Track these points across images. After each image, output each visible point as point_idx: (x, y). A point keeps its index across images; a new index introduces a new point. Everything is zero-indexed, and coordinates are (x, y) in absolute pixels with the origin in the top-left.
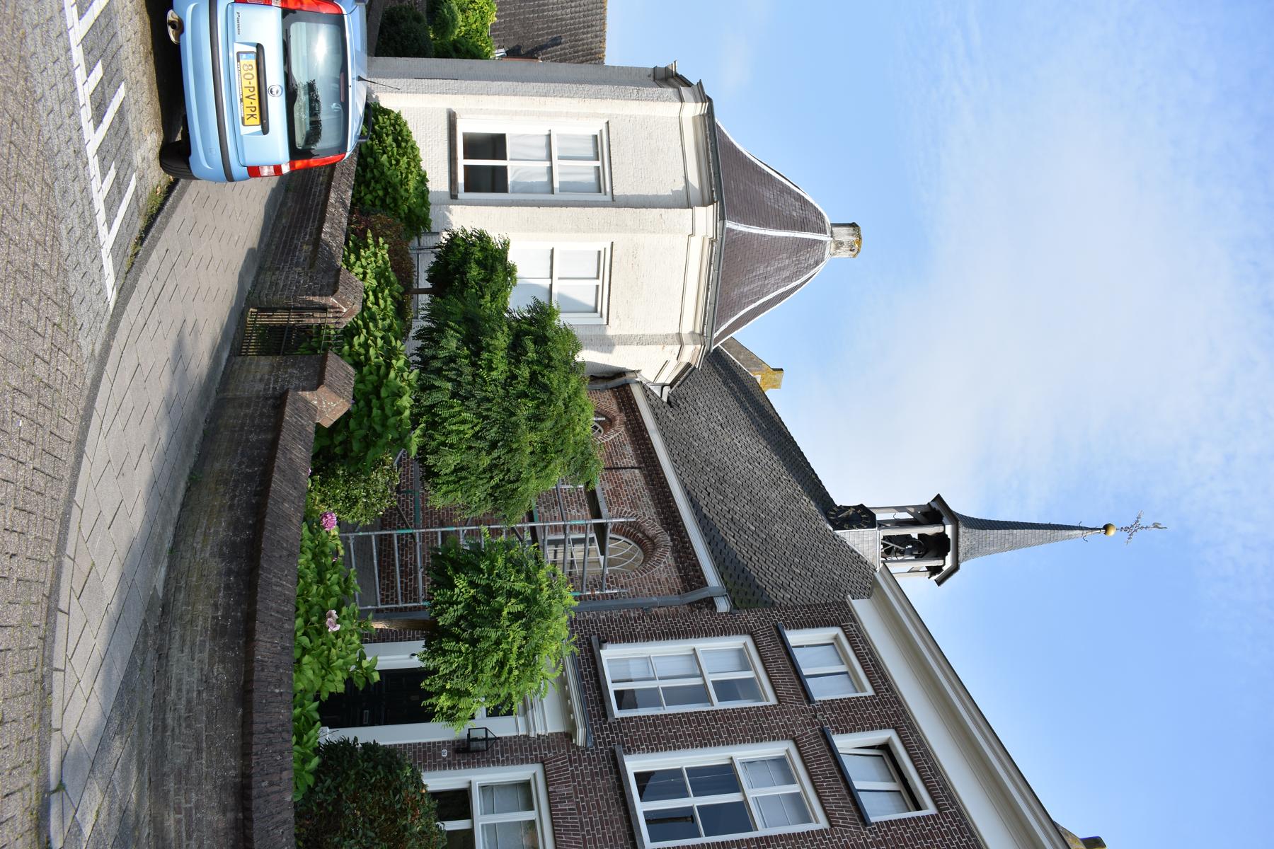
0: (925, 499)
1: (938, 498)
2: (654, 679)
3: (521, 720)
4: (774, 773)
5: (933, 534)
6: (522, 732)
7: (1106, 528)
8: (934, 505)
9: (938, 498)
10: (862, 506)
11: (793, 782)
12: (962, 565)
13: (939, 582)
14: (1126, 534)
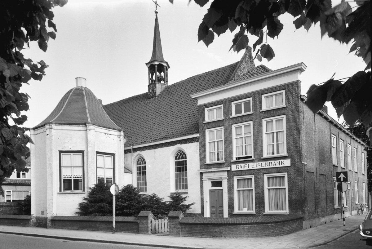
0: (146, 69)
1: (147, 64)
2: (273, 145)
3: (224, 180)
4: (270, 124)
5: (157, 68)
6: (227, 180)
7: (156, 13)
8: (149, 65)
9: (147, 64)
10: (148, 86)
11: (273, 121)
12: (167, 61)
13: (169, 68)
14: (158, 7)
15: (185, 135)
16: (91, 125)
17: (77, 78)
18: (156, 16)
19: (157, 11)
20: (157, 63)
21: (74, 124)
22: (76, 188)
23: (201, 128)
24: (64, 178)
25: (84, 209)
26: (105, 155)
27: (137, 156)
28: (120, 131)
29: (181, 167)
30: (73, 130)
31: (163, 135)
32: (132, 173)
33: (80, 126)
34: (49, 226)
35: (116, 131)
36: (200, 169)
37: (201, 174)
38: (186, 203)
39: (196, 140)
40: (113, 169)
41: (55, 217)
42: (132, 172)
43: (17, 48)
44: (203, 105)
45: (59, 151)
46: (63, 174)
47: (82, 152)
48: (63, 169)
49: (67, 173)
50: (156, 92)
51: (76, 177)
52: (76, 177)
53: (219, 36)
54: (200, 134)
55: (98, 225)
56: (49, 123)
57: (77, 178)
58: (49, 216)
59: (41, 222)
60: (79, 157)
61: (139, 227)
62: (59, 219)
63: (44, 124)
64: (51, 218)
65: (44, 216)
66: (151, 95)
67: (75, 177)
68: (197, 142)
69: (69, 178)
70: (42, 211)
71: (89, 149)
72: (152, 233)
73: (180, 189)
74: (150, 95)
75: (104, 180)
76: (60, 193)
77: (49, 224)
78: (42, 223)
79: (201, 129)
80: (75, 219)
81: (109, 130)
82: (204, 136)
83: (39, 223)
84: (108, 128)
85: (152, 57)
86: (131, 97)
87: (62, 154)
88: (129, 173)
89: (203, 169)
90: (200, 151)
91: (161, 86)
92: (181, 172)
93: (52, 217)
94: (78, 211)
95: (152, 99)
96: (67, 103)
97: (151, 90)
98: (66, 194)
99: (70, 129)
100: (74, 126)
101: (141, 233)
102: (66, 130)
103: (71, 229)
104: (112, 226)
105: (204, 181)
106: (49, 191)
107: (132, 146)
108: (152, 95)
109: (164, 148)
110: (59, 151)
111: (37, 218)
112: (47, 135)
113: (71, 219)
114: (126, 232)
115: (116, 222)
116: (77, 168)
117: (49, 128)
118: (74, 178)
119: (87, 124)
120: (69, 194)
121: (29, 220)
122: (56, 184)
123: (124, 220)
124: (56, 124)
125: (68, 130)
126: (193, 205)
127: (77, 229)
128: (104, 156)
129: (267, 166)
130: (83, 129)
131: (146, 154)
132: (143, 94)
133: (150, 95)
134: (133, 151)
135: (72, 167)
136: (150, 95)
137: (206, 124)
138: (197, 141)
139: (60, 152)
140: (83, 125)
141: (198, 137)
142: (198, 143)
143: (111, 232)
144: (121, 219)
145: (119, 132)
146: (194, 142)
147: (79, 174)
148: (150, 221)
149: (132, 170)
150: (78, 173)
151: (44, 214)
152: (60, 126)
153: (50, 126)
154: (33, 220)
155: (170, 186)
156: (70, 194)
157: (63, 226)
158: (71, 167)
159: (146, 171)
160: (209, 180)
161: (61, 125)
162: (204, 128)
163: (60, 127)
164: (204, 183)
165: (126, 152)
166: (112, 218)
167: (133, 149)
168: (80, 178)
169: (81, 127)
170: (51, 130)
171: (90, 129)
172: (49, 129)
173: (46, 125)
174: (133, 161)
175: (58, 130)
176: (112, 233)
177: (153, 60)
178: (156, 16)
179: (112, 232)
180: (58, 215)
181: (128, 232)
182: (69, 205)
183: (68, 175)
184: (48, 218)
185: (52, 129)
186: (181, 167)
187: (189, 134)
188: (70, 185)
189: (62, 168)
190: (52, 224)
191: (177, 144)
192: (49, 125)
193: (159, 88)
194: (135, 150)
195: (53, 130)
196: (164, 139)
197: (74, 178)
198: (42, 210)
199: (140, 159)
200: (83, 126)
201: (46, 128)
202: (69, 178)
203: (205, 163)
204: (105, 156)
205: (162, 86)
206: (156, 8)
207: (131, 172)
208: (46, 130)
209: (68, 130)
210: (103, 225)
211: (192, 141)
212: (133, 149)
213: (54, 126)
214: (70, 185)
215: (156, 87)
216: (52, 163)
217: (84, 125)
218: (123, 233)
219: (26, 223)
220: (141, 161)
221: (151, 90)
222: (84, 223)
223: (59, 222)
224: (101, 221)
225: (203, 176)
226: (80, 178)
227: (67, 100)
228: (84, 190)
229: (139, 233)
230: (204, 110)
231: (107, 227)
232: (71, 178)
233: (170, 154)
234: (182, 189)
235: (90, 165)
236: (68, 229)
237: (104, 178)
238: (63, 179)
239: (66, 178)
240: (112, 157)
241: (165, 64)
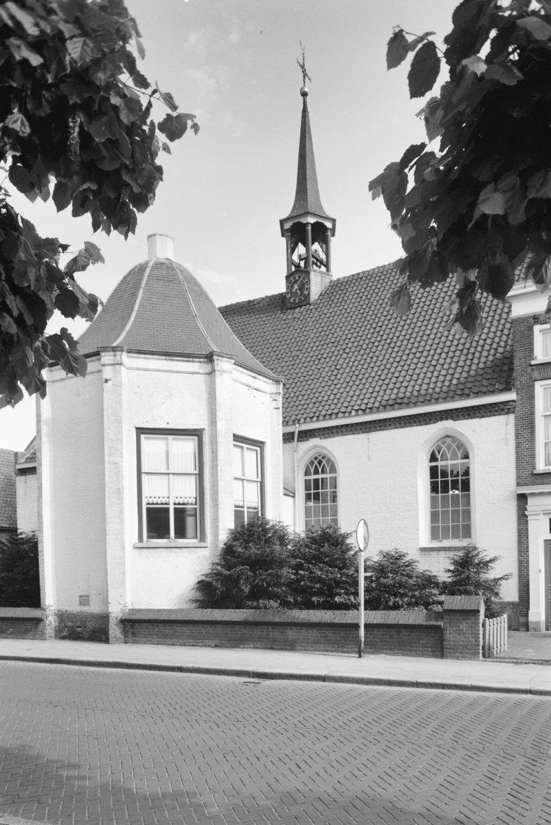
7: (304, 94)
15: (464, 395)
16: (225, 359)
17: (154, 235)
18: (305, 103)
19: (306, 90)
20: (312, 220)
21: (177, 356)
22: (181, 533)
23: (523, 379)
24: (149, 504)
25: (211, 592)
26: (245, 446)
27: (310, 450)
28: (277, 382)
29: (449, 483)
30: (173, 372)
31: (389, 395)
32: (294, 497)
33: (193, 361)
34: (115, 636)
35: (268, 380)
36: (518, 484)
37: (522, 498)
38: (491, 575)
39: (503, 410)
40: (259, 483)
41: (133, 611)
42: (294, 493)
43: (44, 115)
44: (529, 317)
45: (137, 429)
46: (145, 493)
47: (197, 433)
48: (144, 478)
49: (156, 491)
50: (309, 294)
51: (159, 502)
52: (181, 502)
53: (69, 246)
54: (517, 394)
55: (291, 634)
56: (114, 349)
57: (184, 504)
58: (116, 610)
59: (80, 627)
60: (187, 447)
61: (442, 640)
62: (151, 617)
63: (96, 350)
64: (120, 616)
65: (94, 608)
66: (294, 300)
67: (151, 501)
68: (508, 413)
69: (162, 504)
70: (80, 596)
71: (221, 426)
72: (484, 656)
73: (446, 537)
74: (293, 299)
75: (243, 512)
76: (141, 545)
77: (114, 631)
78: (90, 628)
79: (519, 378)
80: (180, 617)
81: (255, 378)
82: (532, 398)
83: (72, 629)
84: (254, 372)
85: (294, 206)
86: (273, 296)
87: (143, 436)
88: (289, 496)
89: (526, 484)
90: (517, 438)
91: (320, 278)
92: (440, 494)
93: (122, 610)
94: (198, 595)
95: (297, 310)
96: (143, 299)
97: (296, 287)
98: (159, 550)
99: (168, 369)
100: (177, 360)
101: (452, 658)
102: (156, 371)
103: (193, 645)
104: (358, 637)
105: (529, 518)
106: (111, 540)
107: (297, 425)
108: (297, 301)
109: (400, 430)
110: (137, 429)
111: (62, 616)
112: (107, 381)
113: (173, 617)
114: (394, 654)
115: (366, 626)
116: (184, 477)
117: (112, 362)
118: (175, 504)
119: (215, 357)
120: (166, 549)
121: (38, 621)
122: (127, 523)
123: (337, 621)
124: (129, 352)
125: (160, 371)
126: (507, 579)
127: (216, 646)
128: (242, 448)
129: (147, 500)
130: (201, 371)
131: (335, 447)
132: (263, 299)
133: (293, 299)
134: (298, 438)
135: (171, 476)
136: (292, 301)
137: (540, 367)
138: (508, 412)
139: (141, 431)
140: (202, 360)
141: (514, 401)
142: (511, 417)
143: (354, 655)
144: (378, 617)
145: (275, 386)
146: (500, 414)
147: (161, 495)
148: (481, 622)
149: (294, 489)
150: (182, 492)
151: (88, 604)
152: (139, 358)
153: (115, 355)
154: (51, 621)
155: (418, 530)
156: (167, 548)
157: (166, 636)
158: (169, 474)
159: (306, 490)
160: (544, 514)
161: (143, 356)
162: (531, 377)
163: (141, 360)
164: (529, 522)
165: (288, 438)
166: (359, 614)
167: (300, 432)
168: (192, 504)
169: (197, 365)
170: (118, 366)
171: (222, 371)
172: (112, 365)
173: (102, 354)
174: (296, 465)
175: (133, 369)
176: (358, 655)
177: (300, 212)
178: (305, 103)
179: (355, 652)
180: (137, 607)
181: (403, 655)
182: (165, 578)
183: (181, 495)
184: (112, 616)
185: (121, 364)
186: (449, 483)
187: (477, 393)
188: (160, 523)
189: (143, 475)
190: (125, 633)
191: (441, 419)
192: (112, 353)
193: (317, 284)
194: (305, 435)
195: (123, 368)
196: (397, 406)
197: (175, 504)
198: (84, 594)
199: (316, 458)
200: (200, 362)
201: (102, 363)
202: (162, 504)
203: (535, 469)
204: (245, 448)
205: (324, 279)
206: (304, 82)
207: (292, 495)
208: (100, 367)
209: (160, 371)
210: (313, 634)
211: (491, 412)
212: (299, 432)
213: (125, 357)
214: (160, 523)
215: (309, 280)
216: (122, 462)
217: (205, 360)
218: (383, 655)
219: (30, 628)
220: (320, 465)
221: (296, 287)
222: (243, 630)
223: (139, 626)
224: (198, 621)
225: (527, 504)
226: (192, 504)
227: (141, 290)
228: (203, 539)
229: (442, 657)
230: (531, 329)
231: (341, 638)
232: (166, 504)
233: (422, 442)
234: (453, 538)
235: (221, 470)
236: (185, 645)
237: (243, 507)
238: (147, 508)
239: (153, 504)
240: (257, 451)
241: (329, 225)
